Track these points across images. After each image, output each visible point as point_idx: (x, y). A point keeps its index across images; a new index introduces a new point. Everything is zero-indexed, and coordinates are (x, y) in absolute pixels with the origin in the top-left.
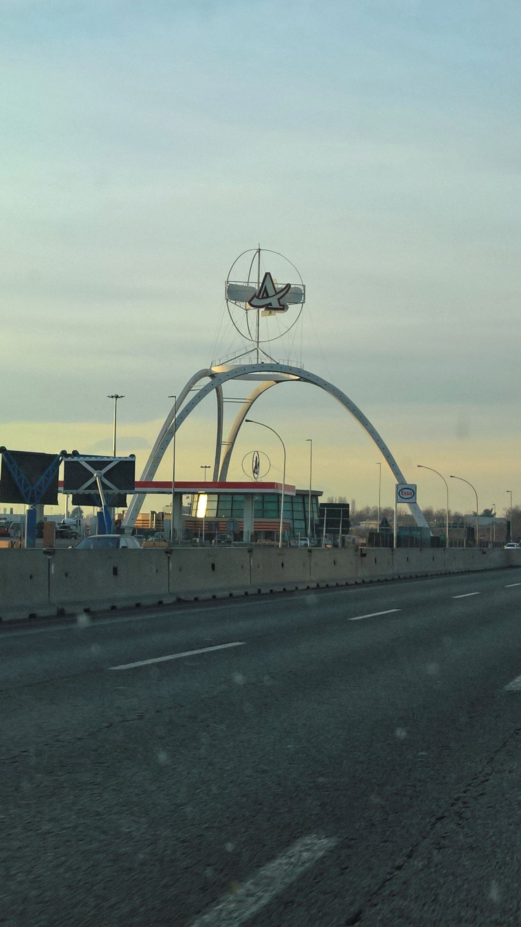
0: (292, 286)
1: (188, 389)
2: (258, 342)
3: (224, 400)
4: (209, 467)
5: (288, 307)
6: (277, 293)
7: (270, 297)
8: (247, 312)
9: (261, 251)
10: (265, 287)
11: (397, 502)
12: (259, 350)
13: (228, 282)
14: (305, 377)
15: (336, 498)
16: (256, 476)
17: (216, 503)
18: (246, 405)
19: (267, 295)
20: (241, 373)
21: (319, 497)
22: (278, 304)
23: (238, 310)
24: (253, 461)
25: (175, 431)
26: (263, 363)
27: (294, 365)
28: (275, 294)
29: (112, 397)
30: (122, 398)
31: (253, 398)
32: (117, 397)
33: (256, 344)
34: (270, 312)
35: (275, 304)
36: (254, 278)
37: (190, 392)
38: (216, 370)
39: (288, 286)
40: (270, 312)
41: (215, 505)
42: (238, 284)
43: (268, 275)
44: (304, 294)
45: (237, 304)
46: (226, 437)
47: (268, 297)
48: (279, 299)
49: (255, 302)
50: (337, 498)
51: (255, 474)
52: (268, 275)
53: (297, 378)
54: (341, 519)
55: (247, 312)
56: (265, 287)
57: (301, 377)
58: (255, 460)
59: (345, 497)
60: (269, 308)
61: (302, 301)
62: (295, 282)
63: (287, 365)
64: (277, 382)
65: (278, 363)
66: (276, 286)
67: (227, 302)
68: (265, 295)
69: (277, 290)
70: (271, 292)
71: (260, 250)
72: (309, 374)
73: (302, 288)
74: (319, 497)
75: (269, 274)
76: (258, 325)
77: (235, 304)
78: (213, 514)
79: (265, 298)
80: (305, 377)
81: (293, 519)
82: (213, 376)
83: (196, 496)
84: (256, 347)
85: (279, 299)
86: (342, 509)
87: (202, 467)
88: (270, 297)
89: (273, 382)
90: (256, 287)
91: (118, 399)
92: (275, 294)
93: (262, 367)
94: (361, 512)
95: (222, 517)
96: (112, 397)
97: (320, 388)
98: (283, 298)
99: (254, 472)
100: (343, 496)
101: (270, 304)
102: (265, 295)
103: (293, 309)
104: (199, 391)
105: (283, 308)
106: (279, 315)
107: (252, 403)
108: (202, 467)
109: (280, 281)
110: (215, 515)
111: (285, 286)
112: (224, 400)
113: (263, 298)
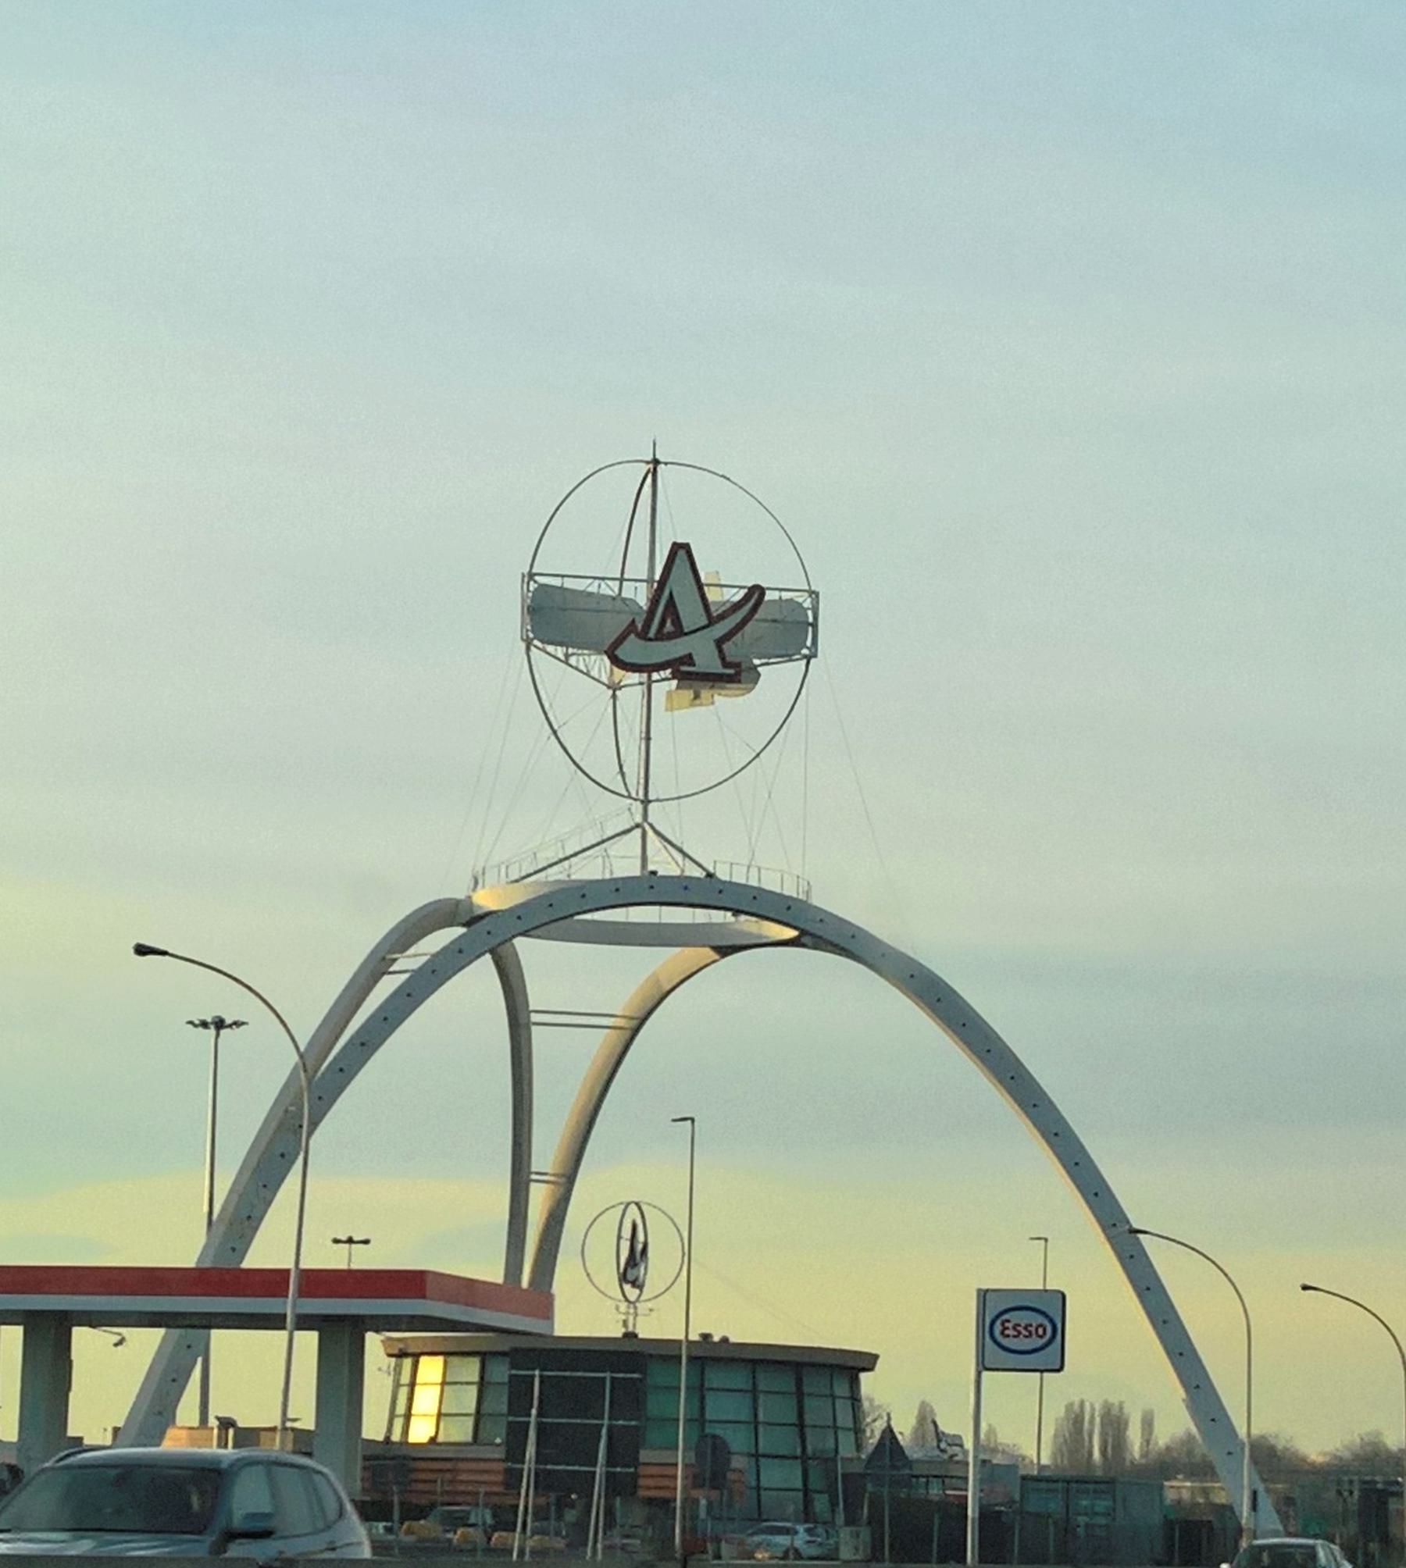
0: (769, 596)
1: (377, 966)
2: (646, 802)
3: (535, 1018)
4: (366, 1242)
5: (759, 675)
6: (712, 621)
7: (692, 634)
8: (614, 696)
9: (661, 468)
10: (671, 594)
11: (983, 1366)
12: (650, 833)
13: (531, 576)
14: (817, 932)
15: (1093, 1409)
16: (632, 1292)
17: (473, 1391)
18: (616, 1038)
19: (677, 622)
20: (562, 911)
21: (863, 1376)
22: (719, 662)
23: (579, 684)
24: (619, 1237)
25: (314, 1125)
26: (654, 873)
27: (771, 884)
28: (704, 621)
29: (204, 1024)
30: (236, 1030)
31: (641, 1014)
32: (220, 1024)
33: (638, 807)
34: (697, 696)
35: (707, 659)
36: (638, 567)
37: (386, 977)
38: (486, 900)
39: (756, 593)
40: (697, 696)
41: (468, 1399)
42: (569, 584)
43: (682, 553)
44: (815, 625)
45: (573, 660)
46: (546, 1155)
47: (679, 632)
48: (720, 643)
49: (632, 649)
50: (1097, 1407)
51: (627, 1287)
52: (681, 551)
53: (792, 933)
54: (606, 1422)
55: (614, 696)
56: (671, 594)
57: (803, 932)
58: (627, 1233)
59: (1121, 1404)
60: (686, 673)
61: (805, 651)
62: (781, 579)
63: (743, 881)
64: (724, 951)
65: (710, 875)
66: (712, 595)
67: (528, 649)
68: (669, 626)
69: (713, 608)
70: (691, 614)
71: (656, 462)
72: (825, 917)
73: (807, 604)
74: (863, 1376)
75: (686, 547)
76: (648, 739)
77: (566, 662)
78: (460, 1432)
79: (671, 636)
80: (817, 932)
81: (756, 1456)
82: (474, 919)
83: (408, 1363)
84: (639, 819)
85: (720, 643)
86: (608, 1375)
87: (336, 1241)
88: (692, 634)
89: (707, 950)
90: (641, 596)
91: (223, 1032)
92: (704, 621)
93: (650, 888)
94: (1168, 1448)
95: (492, 1444)
96: (204, 1024)
97: (861, 966)
98: (738, 637)
99: (623, 1278)
100: (1114, 1399)
101: (689, 659)
102: (669, 626)
103: (777, 677)
104: (406, 976)
105: (735, 675)
106: (725, 703)
107: (636, 1031)
108: (336, 1241)
109: (725, 573)
110: (469, 1438)
111: (743, 592)
112: (535, 1018)
113: (660, 636)
